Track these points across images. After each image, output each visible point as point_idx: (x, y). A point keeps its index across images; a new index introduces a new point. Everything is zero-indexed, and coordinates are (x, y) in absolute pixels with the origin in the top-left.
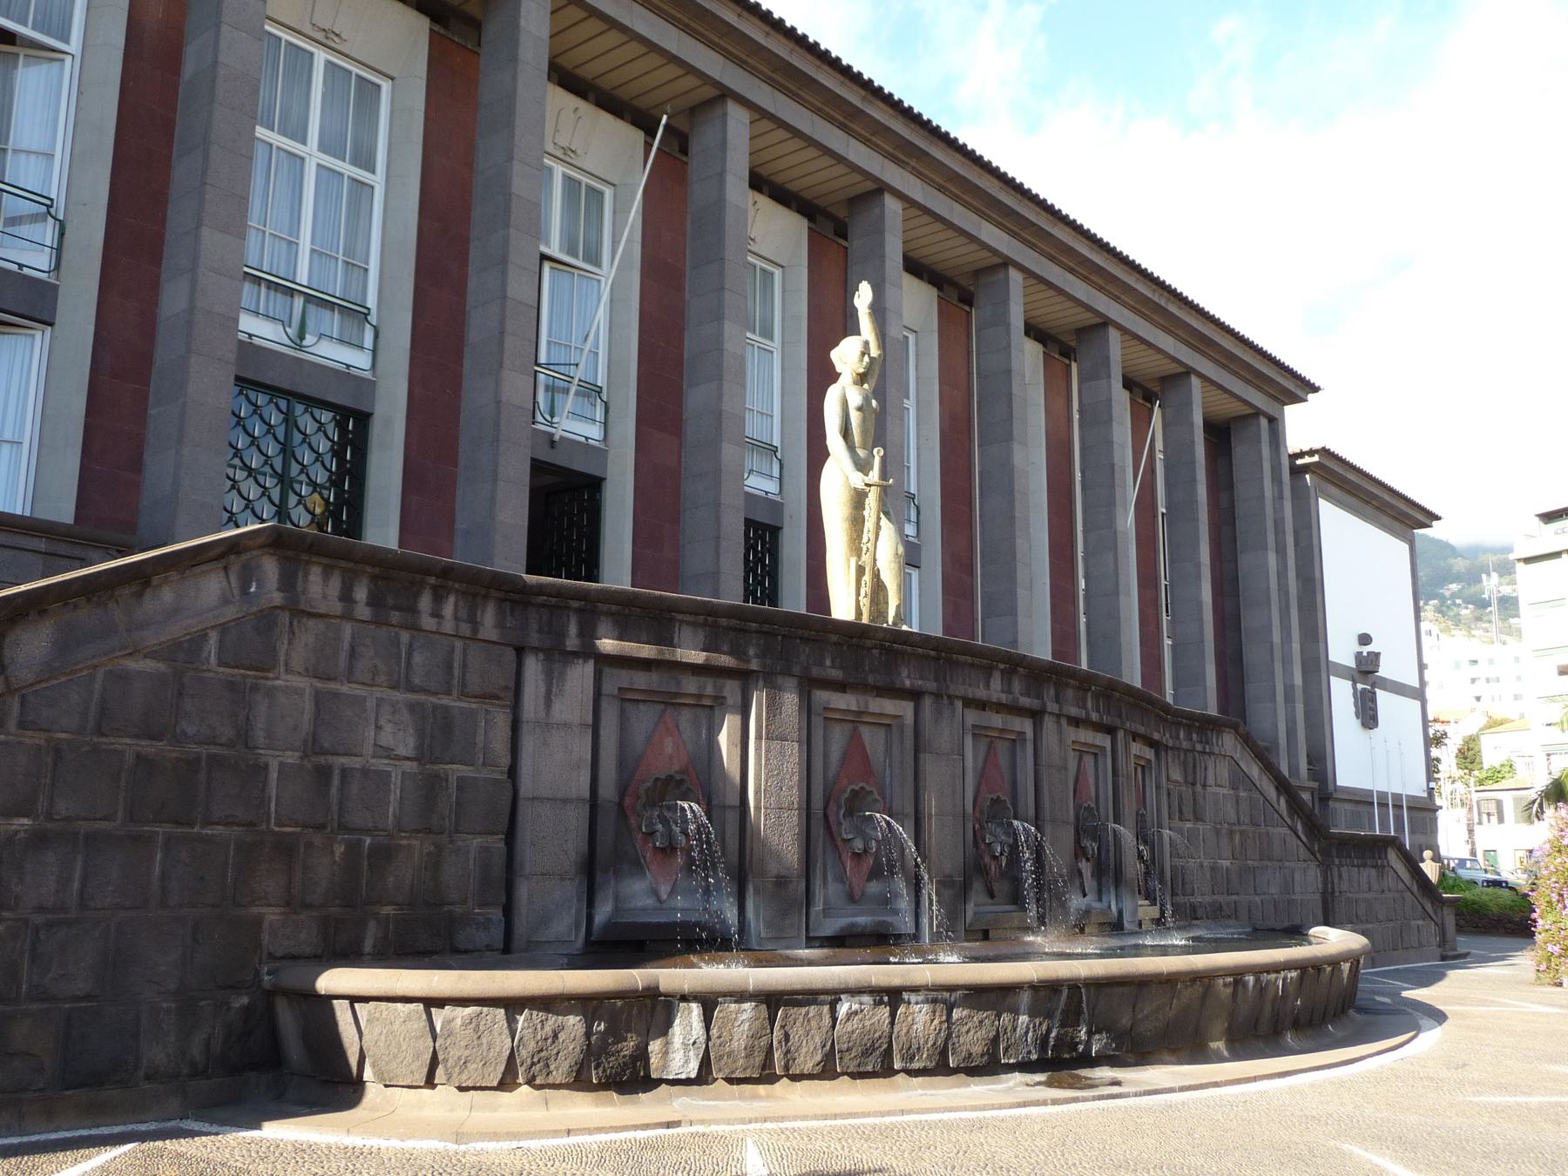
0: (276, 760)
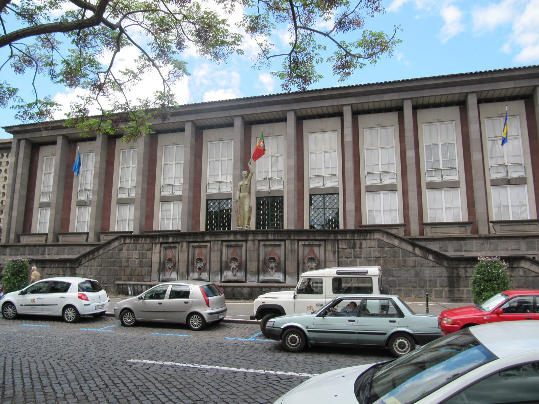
0: (123, 260)
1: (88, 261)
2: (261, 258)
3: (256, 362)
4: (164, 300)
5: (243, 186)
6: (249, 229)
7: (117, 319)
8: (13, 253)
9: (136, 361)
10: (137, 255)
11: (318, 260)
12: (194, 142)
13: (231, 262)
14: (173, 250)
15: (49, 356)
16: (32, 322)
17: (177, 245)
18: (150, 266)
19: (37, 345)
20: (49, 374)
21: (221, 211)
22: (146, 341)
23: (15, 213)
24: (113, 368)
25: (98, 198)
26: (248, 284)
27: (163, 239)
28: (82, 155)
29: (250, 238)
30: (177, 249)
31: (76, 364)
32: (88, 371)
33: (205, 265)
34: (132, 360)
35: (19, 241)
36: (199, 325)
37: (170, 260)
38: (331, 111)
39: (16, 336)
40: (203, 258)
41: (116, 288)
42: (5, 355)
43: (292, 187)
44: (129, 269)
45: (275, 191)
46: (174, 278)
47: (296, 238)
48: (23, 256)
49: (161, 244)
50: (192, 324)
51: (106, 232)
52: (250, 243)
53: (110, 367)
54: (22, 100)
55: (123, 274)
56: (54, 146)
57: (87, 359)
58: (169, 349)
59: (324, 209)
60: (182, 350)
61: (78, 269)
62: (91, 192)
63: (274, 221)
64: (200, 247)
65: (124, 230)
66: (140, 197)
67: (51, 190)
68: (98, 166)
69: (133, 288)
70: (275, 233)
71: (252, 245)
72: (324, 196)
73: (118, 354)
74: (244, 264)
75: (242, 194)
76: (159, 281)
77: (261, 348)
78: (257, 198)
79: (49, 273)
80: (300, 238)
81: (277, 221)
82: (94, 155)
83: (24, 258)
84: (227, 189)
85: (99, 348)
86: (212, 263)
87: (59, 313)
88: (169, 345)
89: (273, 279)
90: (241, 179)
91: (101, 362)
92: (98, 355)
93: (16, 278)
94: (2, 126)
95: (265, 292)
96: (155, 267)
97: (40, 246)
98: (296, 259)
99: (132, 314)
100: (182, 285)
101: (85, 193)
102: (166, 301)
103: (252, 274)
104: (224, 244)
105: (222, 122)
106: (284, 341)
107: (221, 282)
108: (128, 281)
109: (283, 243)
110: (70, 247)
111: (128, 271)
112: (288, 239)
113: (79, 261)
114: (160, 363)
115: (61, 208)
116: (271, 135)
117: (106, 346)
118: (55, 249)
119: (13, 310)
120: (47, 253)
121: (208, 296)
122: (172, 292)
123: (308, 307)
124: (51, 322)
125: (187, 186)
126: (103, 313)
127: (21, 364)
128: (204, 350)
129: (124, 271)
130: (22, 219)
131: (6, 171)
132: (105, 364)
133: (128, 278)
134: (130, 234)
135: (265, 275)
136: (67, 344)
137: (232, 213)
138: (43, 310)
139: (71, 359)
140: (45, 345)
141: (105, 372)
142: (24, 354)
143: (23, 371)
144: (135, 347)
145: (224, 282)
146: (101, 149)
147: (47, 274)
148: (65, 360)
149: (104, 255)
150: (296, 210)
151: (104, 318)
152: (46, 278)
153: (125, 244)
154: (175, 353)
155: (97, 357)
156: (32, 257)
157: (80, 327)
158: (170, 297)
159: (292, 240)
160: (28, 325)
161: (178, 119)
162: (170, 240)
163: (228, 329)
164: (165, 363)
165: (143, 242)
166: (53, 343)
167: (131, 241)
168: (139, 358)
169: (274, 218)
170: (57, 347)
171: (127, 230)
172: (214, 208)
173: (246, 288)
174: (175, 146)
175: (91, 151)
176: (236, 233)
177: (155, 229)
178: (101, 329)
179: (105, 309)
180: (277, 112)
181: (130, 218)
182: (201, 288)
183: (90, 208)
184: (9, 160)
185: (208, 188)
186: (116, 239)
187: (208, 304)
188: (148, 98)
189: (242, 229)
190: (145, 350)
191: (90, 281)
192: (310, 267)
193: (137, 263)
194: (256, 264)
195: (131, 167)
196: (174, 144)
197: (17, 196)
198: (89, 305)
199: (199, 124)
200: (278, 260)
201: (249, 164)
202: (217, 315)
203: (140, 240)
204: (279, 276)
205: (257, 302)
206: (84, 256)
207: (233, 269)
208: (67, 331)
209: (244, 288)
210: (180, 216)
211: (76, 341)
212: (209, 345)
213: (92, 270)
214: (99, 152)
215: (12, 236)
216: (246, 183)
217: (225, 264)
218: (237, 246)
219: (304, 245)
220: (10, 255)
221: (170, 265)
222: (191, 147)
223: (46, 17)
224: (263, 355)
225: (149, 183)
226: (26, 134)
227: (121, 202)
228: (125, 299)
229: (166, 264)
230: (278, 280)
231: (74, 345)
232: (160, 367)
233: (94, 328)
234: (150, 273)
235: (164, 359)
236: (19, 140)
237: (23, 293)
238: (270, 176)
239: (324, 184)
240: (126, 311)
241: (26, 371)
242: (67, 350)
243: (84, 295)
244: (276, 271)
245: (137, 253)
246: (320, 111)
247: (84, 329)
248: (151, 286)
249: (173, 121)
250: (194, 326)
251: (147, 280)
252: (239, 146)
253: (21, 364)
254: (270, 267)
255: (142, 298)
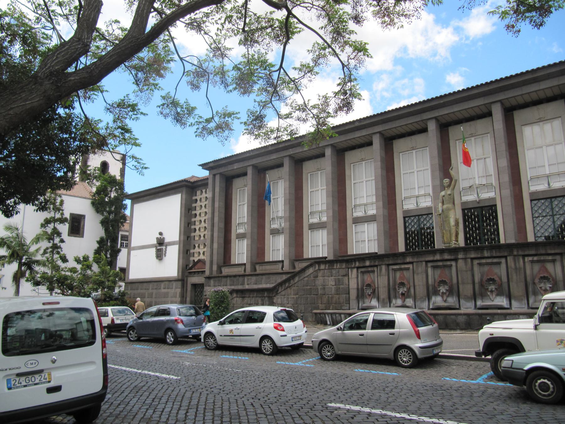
0: (319, 288)
1: (284, 290)
2: (477, 279)
3: (494, 415)
4: (366, 331)
5: (446, 196)
6: (457, 246)
7: (315, 351)
8: (217, 284)
9: (338, 405)
10: (333, 281)
11: (553, 280)
12: (384, 155)
13: (439, 286)
14: (372, 274)
15: (244, 393)
16: (231, 353)
17: (375, 269)
18: (348, 293)
19: (233, 380)
20: (241, 418)
21: (422, 229)
22: (349, 378)
23: (215, 246)
24: (311, 414)
25: (290, 225)
26: (462, 311)
27: (359, 263)
28: (272, 183)
29: (460, 256)
30: (376, 273)
31: (270, 405)
32: (283, 416)
33: (409, 289)
34: (333, 405)
35: (221, 272)
36: (410, 361)
37: (369, 285)
38: (549, 94)
39: (215, 368)
40: (405, 282)
41: (314, 317)
42: (200, 390)
43: (507, 192)
44: (325, 297)
45: (485, 200)
46: (375, 305)
47: (521, 253)
48: (225, 287)
49: (358, 268)
50: (402, 360)
51: (300, 259)
52: (461, 263)
53: (308, 412)
54: (201, 117)
55: (320, 302)
56: (245, 177)
57: (283, 399)
58: (377, 391)
59: (553, 216)
60: (393, 393)
61: (275, 298)
62: (283, 219)
63: (488, 235)
64: (401, 269)
65: (318, 256)
66: (331, 220)
67: (246, 221)
68: (288, 192)
69: (332, 317)
70: (491, 248)
71: (464, 264)
72: (551, 200)
73: (317, 395)
74: (455, 287)
75: (445, 206)
76: (358, 309)
77: (496, 395)
78: (463, 210)
79: (249, 303)
80: (526, 253)
81: (491, 235)
82: (283, 182)
83: (225, 289)
84: (426, 203)
85: (297, 386)
86: (417, 288)
87: (256, 344)
88: (376, 386)
89: (494, 305)
90: (443, 188)
91: (298, 405)
92: (295, 395)
93: (219, 308)
94: (199, 164)
95: (490, 322)
96: (353, 294)
97: (240, 276)
98: (523, 280)
99: (331, 347)
100: (386, 313)
101: (278, 220)
102: (368, 331)
103: (467, 299)
104: (430, 265)
105: (414, 129)
106: (530, 387)
107: (429, 309)
108: (325, 310)
109: (503, 260)
110: (267, 276)
111: (325, 299)
112: (509, 255)
113: (276, 290)
114: (367, 410)
115: (256, 238)
116: (474, 135)
117: (304, 385)
118: (254, 278)
119: (214, 341)
120: (246, 284)
121: (418, 327)
122: (374, 321)
123: (557, 341)
124: (250, 354)
125: (381, 204)
126: (301, 345)
127: (214, 402)
128: (420, 395)
129: (321, 299)
130: (222, 250)
131: (205, 206)
132: (302, 408)
133: (326, 307)
134: (324, 260)
135: (484, 300)
136: (263, 380)
137: (435, 230)
138: (241, 341)
139: (266, 398)
140: (240, 381)
141: (302, 419)
142: (219, 391)
143: (215, 412)
144: (336, 387)
145: (433, 309)
146: (289, 175)
147: (247, 304)
148: (259, 399)
149: (300, 282)
150: (515, 220)
151: (302, 350)
152: (246, 307)
153: (320, 270)
154: (384, 397)
155: (294, 398)
156: (233, 287)
157: (278, 360)
158: (373, 328)
159: (515, 256)
160: (227, 356)
161: (364, 132)
162: (368, 263)
163: (447, 367)
164: (373, 411)
165: (338, 267)
166: (249, 379)
167: (325, 267)
168: (342, 402)
169: (487, 232)
170: (253, 384)
171: (321, 256)
172: (414, 227)
173: (461, 316)
174: (364, 162)
175: (280, 178)
176: (442, 251)
177: (349, 253)
178: (300, 363)
179: (303, 340)
180: (478, 106)
181: (323, 244)
182: (408, 316)
183: (283, 235)
184: (207, 195)
185: (404, 204)
186: (311, 265)
187: (419, 336)
188: (327, 94)
189: (449, 246)
190: (348, 391)
191: (285, 310)
192: (543, 288)
193: (333, 290)
194: (470, 287)
195: (320, 190)
196: (362, 160)
197: (216, 229)
198: (286, 336)
199: (388, 135)
200: (499, 281)
201: (450, 170)
202: (431, 349)
203: (335, 265)
204: (502, 301)
205: (483, 333)
206: (281, 284)
207: (443, 293)
208: (264, 365)
209: (459, 316)
210: (376, 238)
211: (273, 377)
212: (425, 388)
213: (290, 299)
214: (287, 177)
215: (215, 268)
216: (449, 192)
217: (432, 289)
218: (445, 266)
219: (532, 262)
220: (215, 286)
221: (369, 291)
222: (381, 161)
223: (214, 22)
224: (502, 407)
225: (339, 205)
226: (220, 169)
227: (313, 227)
228: (324, 329)
229: (365, 290)
230: (501, 305)
231: (270, 381)
232: (367, 416)
233: (292, 362)
234: (348, 301)
235: (371, 405)
236: (214, 175)
237: (222, 323)
238: (477, 183)
239: (549, 185)
240: (325, 343)
241: (218, 412)
242: (263, 388)
243: (280, 325)
244: (498, 295)
245: (333, 280)
246: (535, 97)
247: (282, 363)
248: (350, 315)
249: (359, 136)
250: (403, 362)
251: (346, 308)
252: (436, 153)
253: (214, 402)
254: (490, 290)
255: (341, 328)
